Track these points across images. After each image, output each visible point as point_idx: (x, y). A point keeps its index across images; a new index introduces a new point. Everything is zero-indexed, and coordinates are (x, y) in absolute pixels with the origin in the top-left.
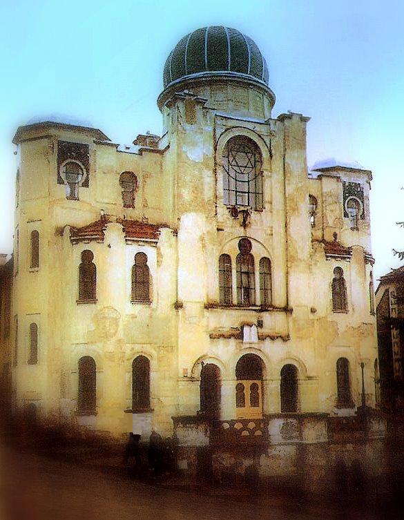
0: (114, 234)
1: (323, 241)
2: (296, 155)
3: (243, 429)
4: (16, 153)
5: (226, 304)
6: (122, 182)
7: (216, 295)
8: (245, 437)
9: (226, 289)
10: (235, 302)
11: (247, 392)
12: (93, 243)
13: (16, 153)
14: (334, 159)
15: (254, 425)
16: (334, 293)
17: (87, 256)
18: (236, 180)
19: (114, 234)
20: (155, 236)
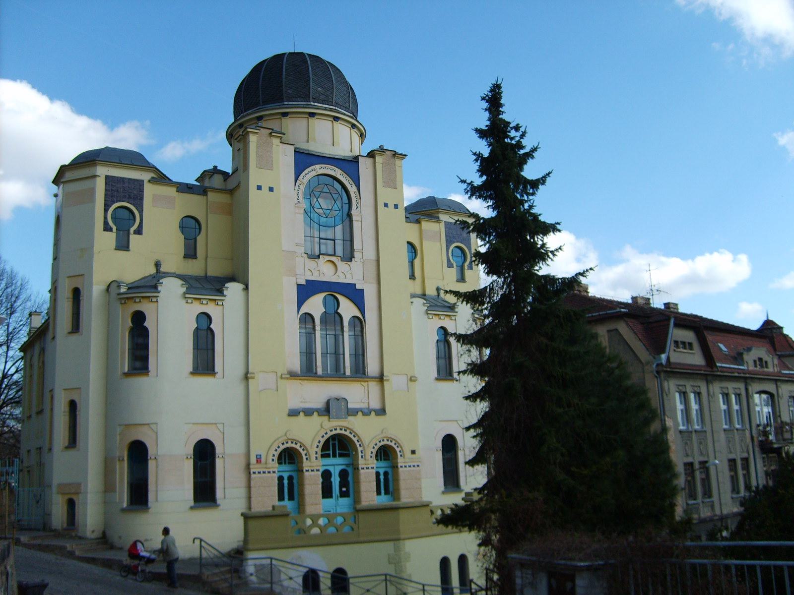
0: (171, 289)
1: (423, 296)
2: (491, 223)
3: (311, 527)
4: (56, 196)
5: (308, 371)
6: (183, 227)
7: (296, 364)
8: (315, 535)
9: (308, 354)
10: (320, 371)
11: (336, 480)
12: (144, 301)
13: (56, 196)
14: (52, 103)
15: (327, 521)
16: (197, 347)
17: (139, 318)
18: (320, 225)
19: (171, 289)
20: (220, 292)
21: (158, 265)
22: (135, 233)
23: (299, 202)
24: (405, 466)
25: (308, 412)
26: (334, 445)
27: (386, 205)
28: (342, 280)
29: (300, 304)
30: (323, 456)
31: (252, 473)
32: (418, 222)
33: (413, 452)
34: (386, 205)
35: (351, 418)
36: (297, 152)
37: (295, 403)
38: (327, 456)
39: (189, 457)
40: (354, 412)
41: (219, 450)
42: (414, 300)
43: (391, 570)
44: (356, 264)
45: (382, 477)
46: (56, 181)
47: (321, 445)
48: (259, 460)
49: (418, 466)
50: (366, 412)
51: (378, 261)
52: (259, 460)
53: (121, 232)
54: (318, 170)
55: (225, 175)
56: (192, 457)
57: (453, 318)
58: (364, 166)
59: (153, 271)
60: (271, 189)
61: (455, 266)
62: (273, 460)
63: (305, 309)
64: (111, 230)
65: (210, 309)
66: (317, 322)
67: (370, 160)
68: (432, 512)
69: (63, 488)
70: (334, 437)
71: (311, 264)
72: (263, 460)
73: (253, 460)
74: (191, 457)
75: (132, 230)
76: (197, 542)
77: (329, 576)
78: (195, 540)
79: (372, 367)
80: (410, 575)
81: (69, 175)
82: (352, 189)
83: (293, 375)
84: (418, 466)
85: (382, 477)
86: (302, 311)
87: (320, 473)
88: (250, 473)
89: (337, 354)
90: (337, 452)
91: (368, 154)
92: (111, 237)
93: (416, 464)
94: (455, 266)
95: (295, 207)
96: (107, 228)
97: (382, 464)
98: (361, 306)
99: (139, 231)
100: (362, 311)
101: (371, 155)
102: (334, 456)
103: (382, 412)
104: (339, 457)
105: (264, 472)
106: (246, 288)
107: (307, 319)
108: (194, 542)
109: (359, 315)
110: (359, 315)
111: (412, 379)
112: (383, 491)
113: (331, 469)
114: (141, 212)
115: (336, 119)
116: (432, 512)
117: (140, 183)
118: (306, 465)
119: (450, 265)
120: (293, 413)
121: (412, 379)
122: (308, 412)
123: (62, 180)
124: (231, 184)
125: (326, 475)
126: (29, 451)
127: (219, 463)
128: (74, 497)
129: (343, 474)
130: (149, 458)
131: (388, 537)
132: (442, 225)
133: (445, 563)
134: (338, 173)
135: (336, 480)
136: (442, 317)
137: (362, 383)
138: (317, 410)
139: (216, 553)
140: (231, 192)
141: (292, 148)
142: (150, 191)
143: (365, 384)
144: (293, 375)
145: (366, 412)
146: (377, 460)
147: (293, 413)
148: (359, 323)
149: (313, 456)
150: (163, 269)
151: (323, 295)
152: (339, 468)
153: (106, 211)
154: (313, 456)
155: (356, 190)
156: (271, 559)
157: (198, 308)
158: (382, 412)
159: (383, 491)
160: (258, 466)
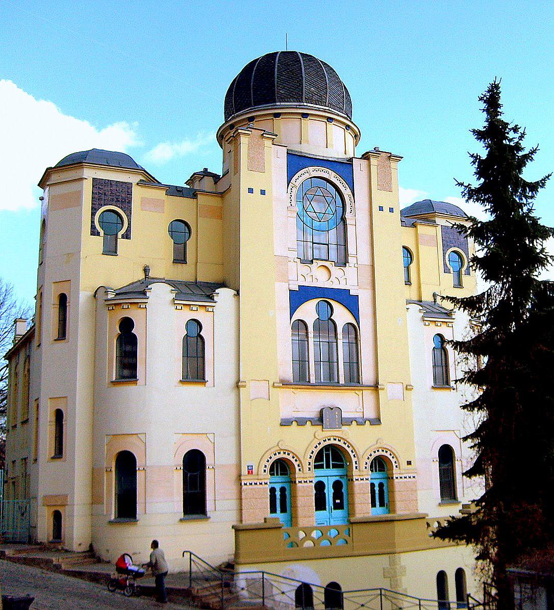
4: (42, 199)
7: (288, 372)
11: (329, 492)
13: (42, 199)
21: (146, 270)
22: (123, 237)
23: (291, 205)
24: (401, 478)
25: (301, 422)
26: (328, 456)
27: (381, 209)
28: (336, 286)
29: (293, 310)
30: (316, 467)
31: (243, 484)
32: (414, 225)
33: (409, 463)
34: (381, 209)
35: (344, 428)
36: (290, 154)
37: (288, 412)
38: (321, 467)
39: (179, 468)
40: (348, 422)
41: (209, 461)
42: (409, 306)
43: (386, 584)
44: (350, 270)
45: (377, 489)
46: (42, 184)
47: (314, 456)
48: (250, 472)
49: (414, 477)
50: (361, 422)
51: (373, 266)
52: (250, 472)
53: (109, 236)
54: (311, 171)
55: (216, 178)
56: (182, 468)
57: (450, 325)
58: (359, 168)
59: (142, 276)
60: (263, 192)
61: (452, 271)
62: (265, 471)
63: (298, 315)
64: (98, 234)
65: (201, 315)
66: (311, 329)
67: (364, 163)
68: (428, 525)
69: (49, 500)
70: (327, 448)
71: (304, 269)
72: (255, 471)
73: (244, 471)
74: (180, 468)
75: (120, 235)
76: (187, 555)
77: (323, 590)
78: (185, 553)
79: (367, 376)
80: (406, 590)
81: (55, 178)
82: (346, 192)
83: (285, 384)
84: (414, 477)
85: (377, 489)
86: (294, 318)
87: (313, 484)
88: (241, 484)
89: (331, 362)
90: (331, 462)
91: (363, 156)
92: (99, 241)
93: (412, 475)
94: (452, 271)
95: (288, 210)
96: (94, 232)
97: (377, 475)
98: (355, 312)
99: (127, 236)
100: (357, 318)
101: (366, 157)
102: (328, 467)
103: (377, 421)
104: (333, 467)
105: (256, 484)
106: (238, 294)
107: (300, 325)
108: (183, 556)
109: (354, 322)
110: (354, 322)
111: (408, 388)
112: (378, 503)
113: (324, 480)
114: (129, 216)
115: (330, 120)
116: (428, 525)
117: (128, 186)
118: (299, 476)
119: (447, 271)
120: (286, 423)
121: (408, 388)
122: (301, 422)
123: (48, 183)
124: (222, 187)
125: (320, 486)
126: (14, 462)
127: (209, 474)
128: (61, 510)
129: (337, 486)
130: (137, 469)
131: (383, 551)
132: (439, 228)
133: (441, 577)
134: (332, 176)
135: (329, 492)
136: (439, 324)
137: (356, 392)
138: (310, 420)
139: (207, 567)
140: (222, 195)
141: (285, 150)
142: (138, 193)
143: (360, 393)
144: (285, 384)
145: (361, 422)
146: (372, 471)
147: (286, 423)
148: (353, 329)
149: (306, 467)
150: (151, 275)
151: (316, 301)
152: (332, 480)
153: (93, 214)
154: (306, 467)
155: (351, 193)
156: (263, 573)
157: (188, 315)
158: (377, 421)
159: (378, 503)
160: (250, 477)
